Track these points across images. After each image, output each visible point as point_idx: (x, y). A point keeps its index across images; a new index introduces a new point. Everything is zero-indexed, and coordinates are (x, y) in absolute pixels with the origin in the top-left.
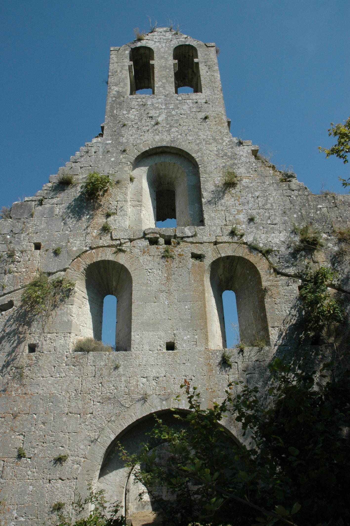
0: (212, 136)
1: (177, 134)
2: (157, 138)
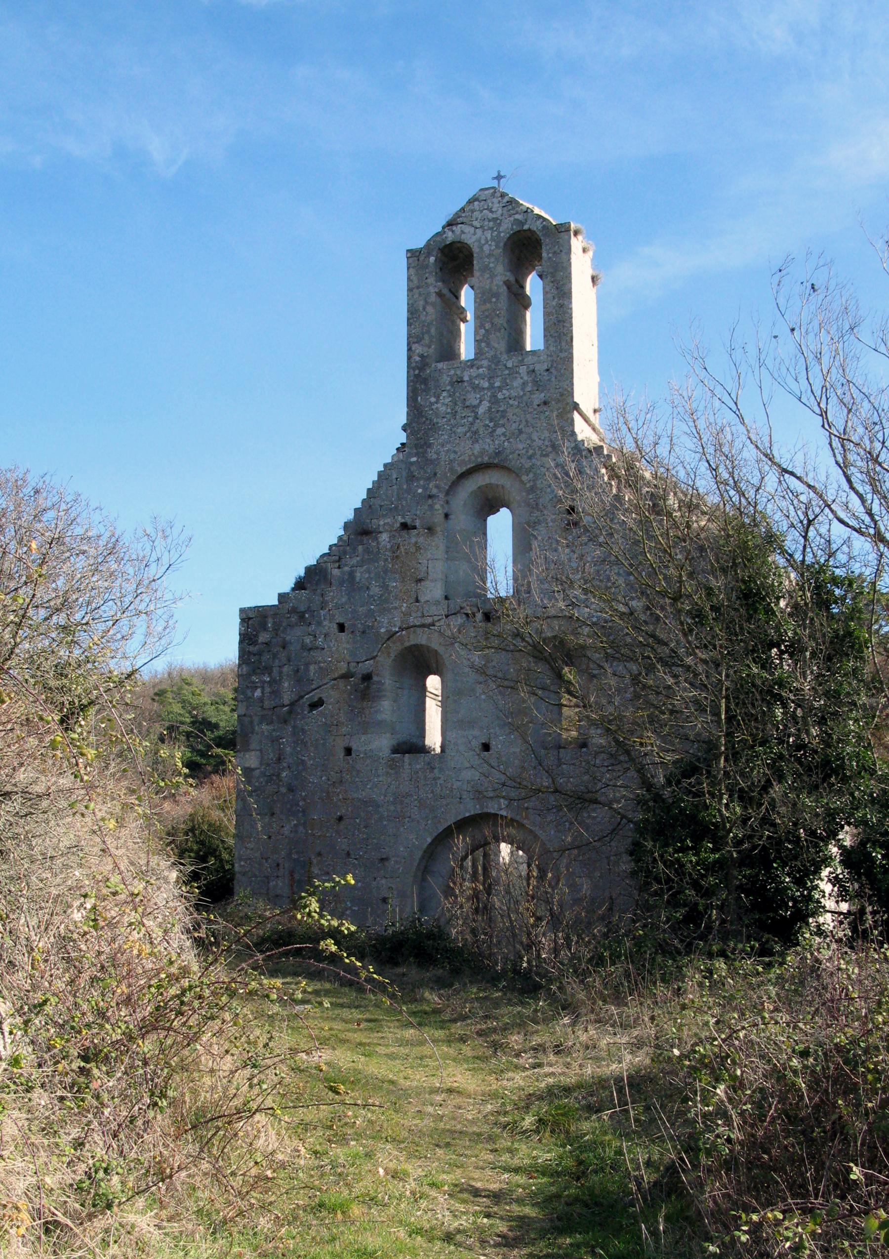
0: (551, 441)
1: (503, 438)
2: (477, 448)
